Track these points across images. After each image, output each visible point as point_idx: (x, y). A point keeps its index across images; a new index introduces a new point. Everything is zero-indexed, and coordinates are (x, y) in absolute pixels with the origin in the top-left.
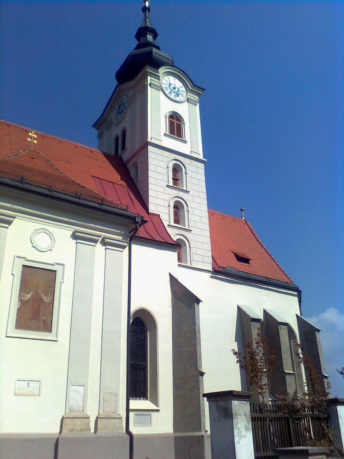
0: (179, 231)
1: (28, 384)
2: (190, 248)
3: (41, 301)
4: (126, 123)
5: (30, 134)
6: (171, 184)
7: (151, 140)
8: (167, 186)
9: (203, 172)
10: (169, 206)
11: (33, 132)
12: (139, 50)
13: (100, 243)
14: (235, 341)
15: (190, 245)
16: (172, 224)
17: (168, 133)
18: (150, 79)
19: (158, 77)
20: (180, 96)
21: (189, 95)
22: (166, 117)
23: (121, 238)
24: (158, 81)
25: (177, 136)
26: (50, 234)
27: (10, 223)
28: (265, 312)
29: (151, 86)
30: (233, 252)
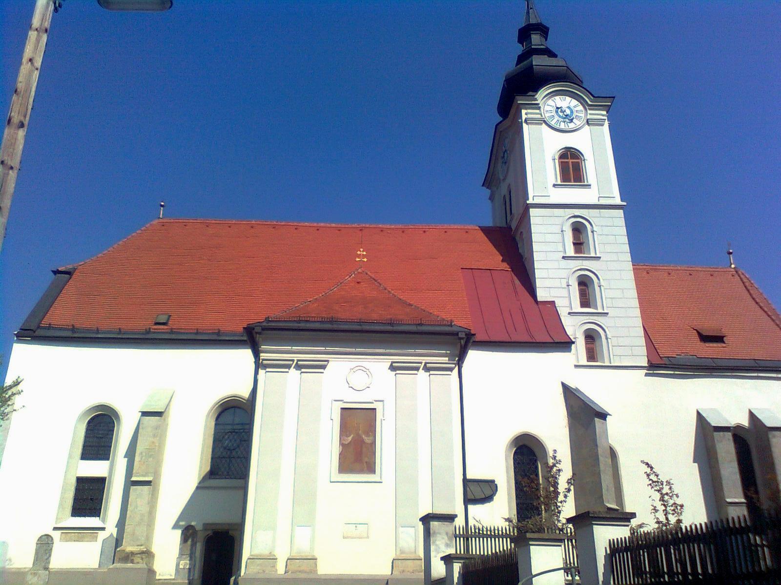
0: (588, 317)
1: (356, 527)
2: (607, 338)
3: (363, 441)
4: (510, 180)
5: (359, 253)
6: (571, 251)
7: (533, 200)
8: (564, 258)
9: (622, 222)
10: (568, 286)
11: (362, 250)
12: (522, 64)
13: (423, 369)
14: (694, 462)
15: (606, 336)
16: (577, 308)
17: (559, 182)
18: (525, 113)
19: (537, 106)
20: (574, 121)
21: (590, 114)
22: (554, 159)
23: (447, 359)
24: (538, 111)
25: (574, 182)
26: (365, 370)
27: (324, 367)
28: (751, 414)
29: (527, 123)
30: (694, 330)
